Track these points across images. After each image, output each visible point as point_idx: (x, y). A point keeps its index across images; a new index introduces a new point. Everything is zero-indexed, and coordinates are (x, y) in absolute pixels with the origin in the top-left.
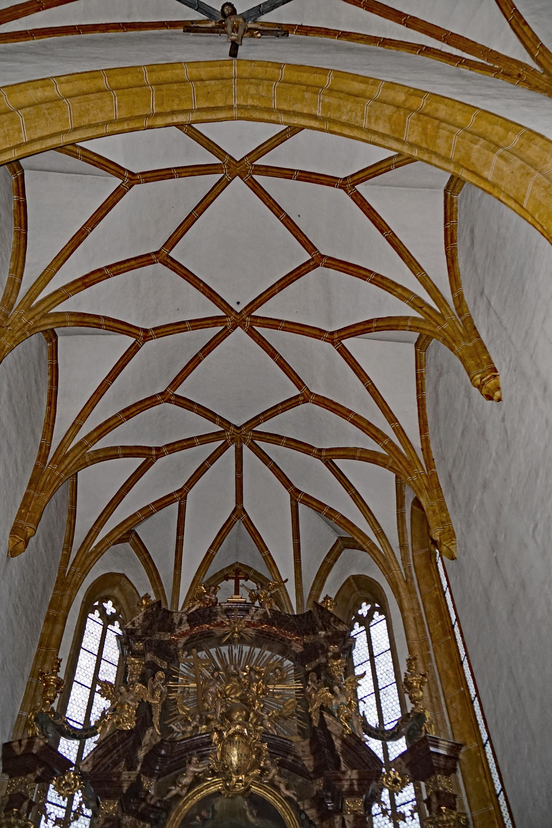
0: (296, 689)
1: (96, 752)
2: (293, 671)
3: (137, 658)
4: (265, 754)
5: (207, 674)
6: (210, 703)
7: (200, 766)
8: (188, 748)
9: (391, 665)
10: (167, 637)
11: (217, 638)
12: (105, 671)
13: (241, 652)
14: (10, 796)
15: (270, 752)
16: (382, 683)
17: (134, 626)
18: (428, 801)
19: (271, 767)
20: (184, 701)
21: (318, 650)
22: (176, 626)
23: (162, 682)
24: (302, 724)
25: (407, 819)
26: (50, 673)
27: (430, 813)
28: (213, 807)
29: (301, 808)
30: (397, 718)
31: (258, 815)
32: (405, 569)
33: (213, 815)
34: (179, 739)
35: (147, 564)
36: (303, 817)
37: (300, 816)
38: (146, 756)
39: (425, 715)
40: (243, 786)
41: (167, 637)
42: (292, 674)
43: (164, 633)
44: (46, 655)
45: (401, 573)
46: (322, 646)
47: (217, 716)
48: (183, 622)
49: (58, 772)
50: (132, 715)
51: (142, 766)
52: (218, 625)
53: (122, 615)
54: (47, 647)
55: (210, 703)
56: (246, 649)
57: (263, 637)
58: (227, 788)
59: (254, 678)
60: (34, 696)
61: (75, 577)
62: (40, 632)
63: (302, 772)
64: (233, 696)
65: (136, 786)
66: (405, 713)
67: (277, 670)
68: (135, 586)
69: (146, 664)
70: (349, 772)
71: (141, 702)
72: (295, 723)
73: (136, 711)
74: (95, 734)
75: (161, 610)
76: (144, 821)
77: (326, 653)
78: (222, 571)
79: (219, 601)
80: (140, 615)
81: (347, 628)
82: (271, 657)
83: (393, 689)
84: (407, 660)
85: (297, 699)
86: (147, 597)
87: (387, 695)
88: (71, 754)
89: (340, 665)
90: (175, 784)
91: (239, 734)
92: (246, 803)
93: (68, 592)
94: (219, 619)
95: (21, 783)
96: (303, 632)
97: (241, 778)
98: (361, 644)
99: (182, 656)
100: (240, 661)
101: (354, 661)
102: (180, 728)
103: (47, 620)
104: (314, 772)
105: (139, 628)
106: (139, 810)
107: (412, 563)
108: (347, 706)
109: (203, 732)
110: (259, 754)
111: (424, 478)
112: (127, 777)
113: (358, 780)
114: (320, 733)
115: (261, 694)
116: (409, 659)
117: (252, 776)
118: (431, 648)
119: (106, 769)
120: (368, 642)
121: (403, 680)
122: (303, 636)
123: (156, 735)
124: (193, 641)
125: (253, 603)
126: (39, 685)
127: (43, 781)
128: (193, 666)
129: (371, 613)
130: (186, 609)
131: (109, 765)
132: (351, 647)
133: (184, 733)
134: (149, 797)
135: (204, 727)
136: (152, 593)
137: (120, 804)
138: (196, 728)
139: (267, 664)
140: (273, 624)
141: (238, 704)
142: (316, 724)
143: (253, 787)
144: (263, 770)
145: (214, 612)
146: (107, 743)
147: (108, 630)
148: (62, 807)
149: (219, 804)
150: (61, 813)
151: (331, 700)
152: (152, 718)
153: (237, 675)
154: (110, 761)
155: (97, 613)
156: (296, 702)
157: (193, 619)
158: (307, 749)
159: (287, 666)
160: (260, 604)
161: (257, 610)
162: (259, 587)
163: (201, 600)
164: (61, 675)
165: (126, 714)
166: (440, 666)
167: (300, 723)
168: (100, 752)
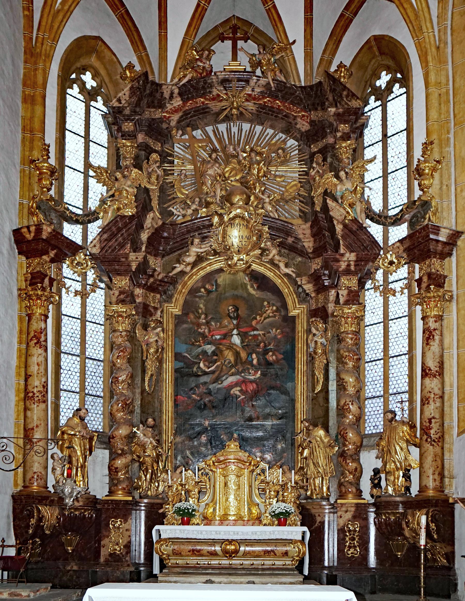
0: (299, 171)
1: (101, 236)
2: (297, 152)
3: (129, 139)
4: (266, 236)
5: (205, 155)
6: (209, 187)
7: (203, 246)
8: (189, 230)
9: (405, 147)
10: (158, 114)
11: (214, 114)
12: (95, 154)
13: (240, 130)
14: (31, 273)
15: (270, 234)
16: (392, 166)
17: (121, 103)
18: (419, 281)
19: (272, 248)
20: (182, 184)
21: (326, 129)
22: (167, 101)
23: (157, 165)
24: (304, 208)
25: (397, 294)
26: (41, 160)
27: (419, 290)
28: (216, 281)
29: (299, 283)
30: (403, 203)
31: (259, 288)
32: (439, 31)
33: (216, 288)
34: (180, 222)
35: (126, 21)
36: (300, 290)
37: (298, 289)
38: (149, 238)
39: (430, 204)
40: (244, 264)
41: (158, 114)
42: (295, 155)
43: (153, 110)
44: (32, 141)
45: (434, 36)
46: (331, 125)
47: (216, 199)
48: (174, 95)
49: (69, 254)
50: (131, 200)
51: (146, 247)
52: (213, 99)
53: (104, 89)
54: (31, 131)
55: (209, 187)
56: (246, 126)
57: (264, 113)
58: (229, 265)
59: (254, 160)
60: (30, 184)
61: (44, 47)
62: (20, 115)
63: (302, 252)
64: (232, 179)
65: (144, 265)
66: (412, 200)
67: (280, 151)
68: (115, 51)
69: (138, 146)
70: (347, 255)
71: (139, 188)
72: (295, 207)
73: (135, 196)
74: (97, 219)
75: (148, 83)
76: (153, 293)
77: (335, 133)
78: (216, 28)
79: (214, 70)
80: (125, 90)
81: (361, 103)
82: (274, 136)
83: (403, 174)
84: (423, 145)
85: (300, 182)
86: (130, 66)
87: (395, 179)
88: (76, 236)
89: (349, 147)
90: (178, 262)
91: (240, 217)
92: (247, 278)
93: (41, 66)
94: (215, 92)
95: (38, 264)
96: (310, 107)
97: (242, 257)
98: (375, 121)
99: (176, 135)
100: (239, 141)
101: (365, 142)
102: (179, 211)
103: (25, 100)
104: (314, 252)
105: (126, 105)
106: (149, 284)
107: (449, 23)
108: (351, 192)
109: (203, 215)
110: (260, 237)
112: (134, 258)
113: (356, 261)
114: (322, 218)
115: (262, 177)
116: (425, 143)
117: (253, 256)
118: (452, 131)
119: (113, 251)
120: (382, 120)
121: (415, 166)
122: (310, 111)
123: (157, 218)
124: (186, 118)
125: (254, 72)
126: (32, 172)
127: (58, 262)
128: (189, 146)
130: (176, 80)
131: (115, 247)
132: (364, 126)
133: (184, 216)
134: (156, 273)
135: (204, 210)
136: (135, 61)
137: (131, 279)
138: (196, 211)
139: (268, 144)
140: (276, 98)
141: (237, 186)
142: (318, 209)
143: (254, 265)
144: (264, 250)
145: (209, 84)
146: (110, 228)
147: (91, 108)
148: (78, 281)
149: (221, 279)
150: (78, 287)
151: (336, 185)
152: (151, 202)
153: (237, 156)
154: (116, 244)
156: (299, 185)
158: (308, 232)
159: (290, 146)
160: (263, 73)
161: (258, 80)
162: (261, 51)
163: (193, 68)
164: (52, 161)
165: (125, 200)
166: (458, 152)
167: (302, 206)
168: (105, 236)
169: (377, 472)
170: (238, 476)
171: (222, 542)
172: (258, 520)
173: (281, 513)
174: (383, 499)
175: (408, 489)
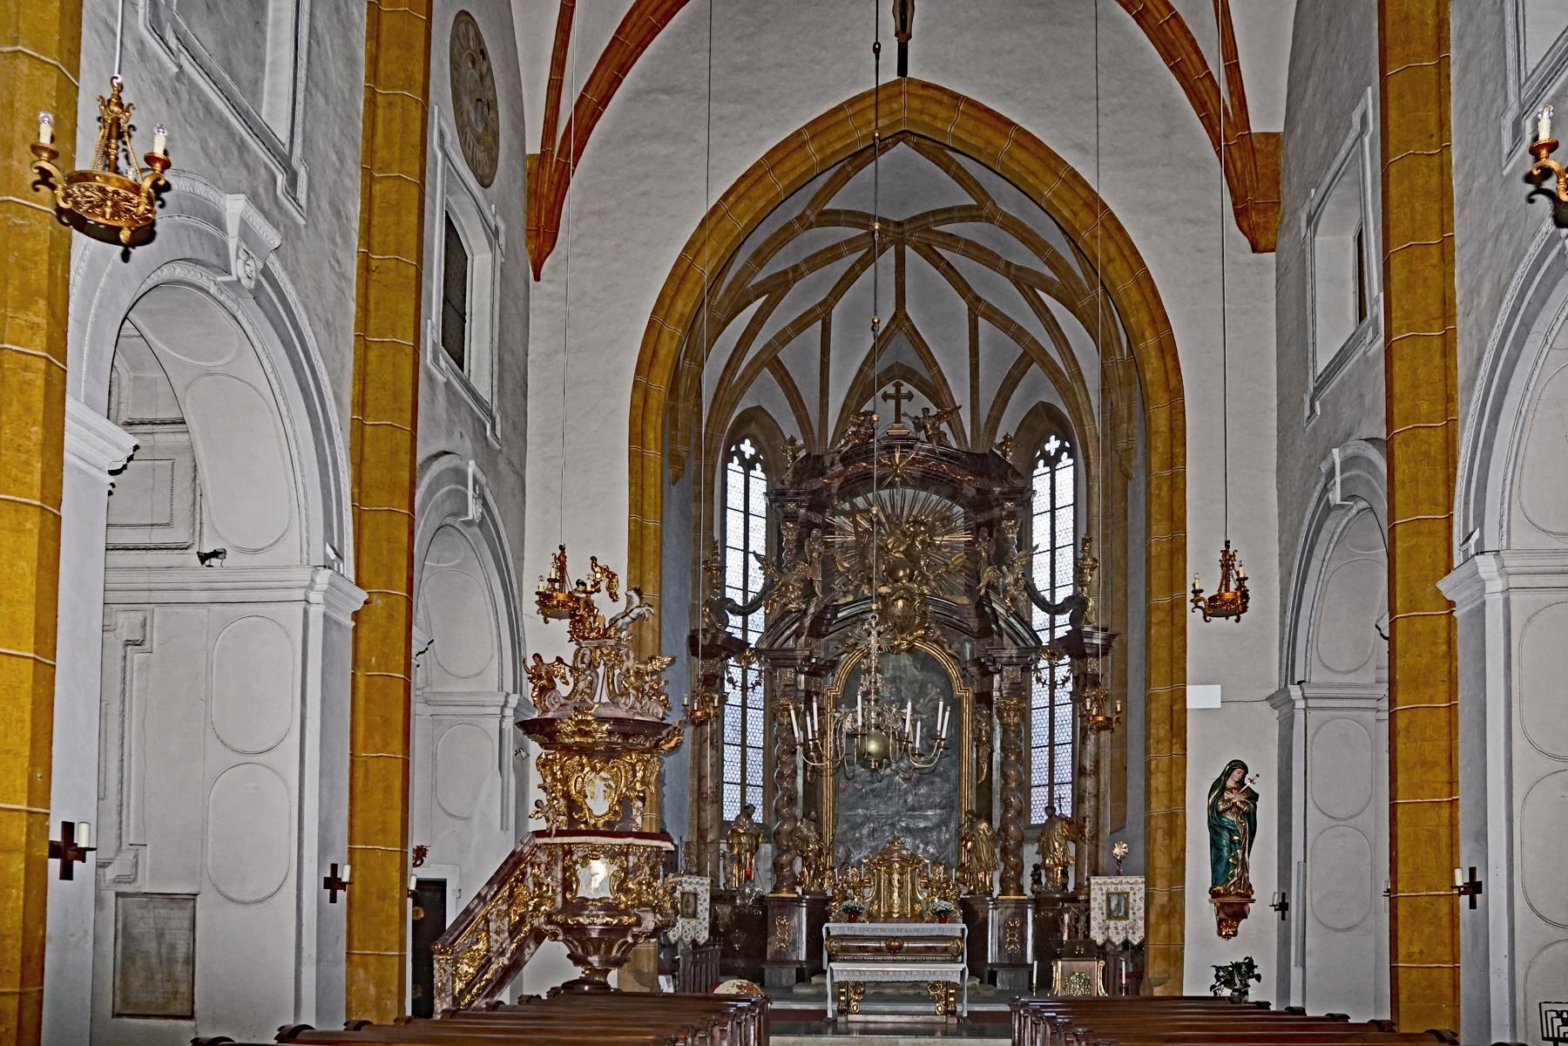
31: (922, 669)
56: (910, 492)
83: (1069, 551)
111: (1120, 366)
129: (1059, 451)
139: (934, 511)
155: (736, 459)
157: (846, 459)
169: (1036, 867)
170: (901, 874)
171: (886, 938)
172: (919, 918)
173: (941, 911)
174: (1042, 895)
175: (1065, 886)
